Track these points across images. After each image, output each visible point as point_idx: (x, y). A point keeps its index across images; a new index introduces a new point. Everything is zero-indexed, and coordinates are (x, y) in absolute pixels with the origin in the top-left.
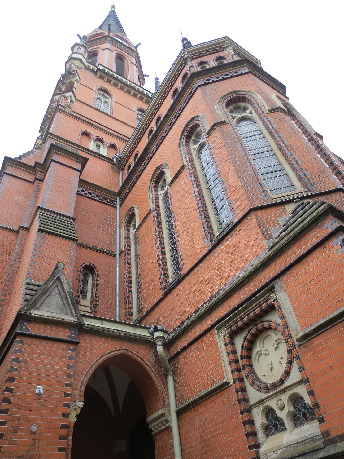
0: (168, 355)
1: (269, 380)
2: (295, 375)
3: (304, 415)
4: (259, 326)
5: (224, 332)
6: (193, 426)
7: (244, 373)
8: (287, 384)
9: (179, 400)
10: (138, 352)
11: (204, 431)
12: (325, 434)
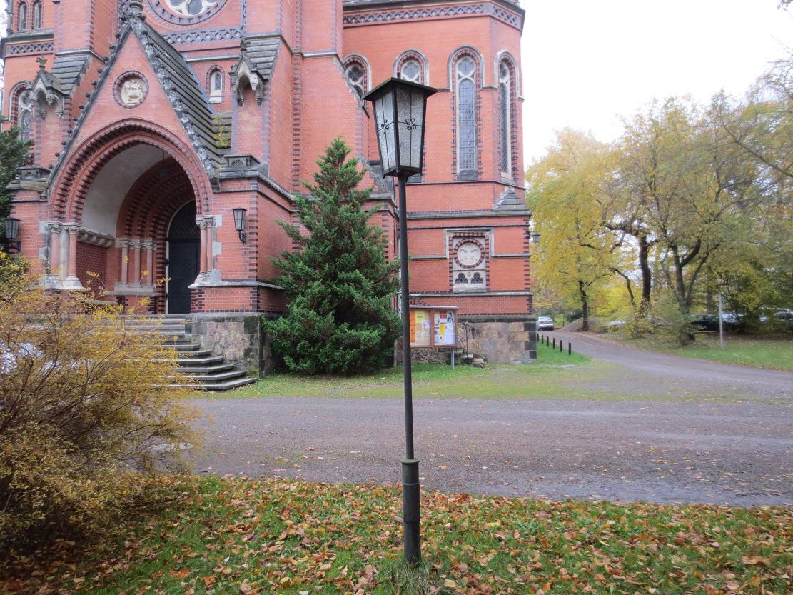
5: (451, 235)
8: (475, 269)
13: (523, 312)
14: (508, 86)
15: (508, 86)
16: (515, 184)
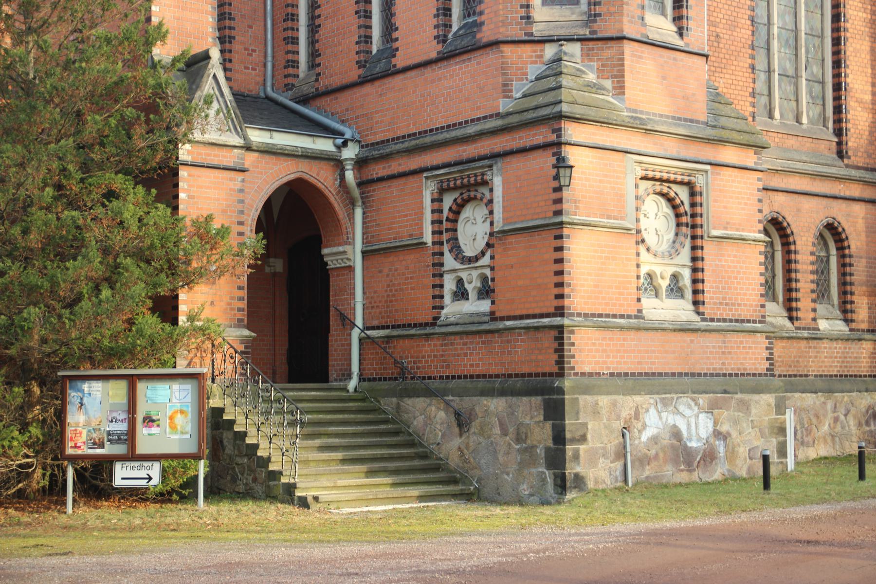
0: (359, 176)
1: (469, 252)
2: (486, 260)
3: (487, 292)
4: (472, 194)
6: (380, 272)
7: (445, 237)
9: (366, 239)
10: (318, 175)
11: (391, 281)
12: (492, 313)
13: (547, 370)
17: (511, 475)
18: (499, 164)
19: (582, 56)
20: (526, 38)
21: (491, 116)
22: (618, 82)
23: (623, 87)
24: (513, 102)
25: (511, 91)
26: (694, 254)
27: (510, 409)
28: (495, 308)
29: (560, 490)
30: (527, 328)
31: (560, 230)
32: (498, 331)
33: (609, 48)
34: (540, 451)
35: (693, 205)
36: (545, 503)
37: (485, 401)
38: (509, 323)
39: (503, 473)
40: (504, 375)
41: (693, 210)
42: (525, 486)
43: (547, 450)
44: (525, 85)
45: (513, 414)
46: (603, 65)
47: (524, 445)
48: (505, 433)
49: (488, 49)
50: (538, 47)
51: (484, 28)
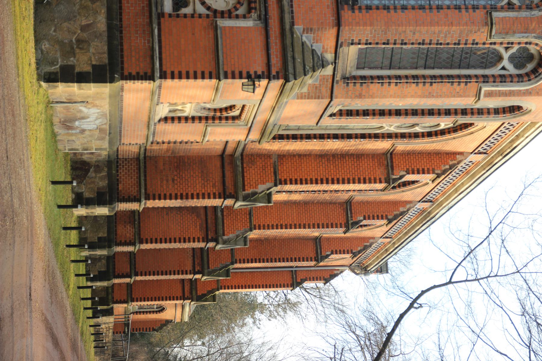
13: (126, 66)
14: (495, 71)
15: (495, 71)
16: (338, 77)
17: (54, 34)
18: (261, 25)
19: (324, 75)
20: (339, 43)
21: (293, 17)
22: (305, 96)
23: (302, 98)
24: (300, 33)
25: (307, 33)
26: (197, 118)
27: (98, 35)
28: (167, 16)
29: (47, 77)
30: (152, 49)
31: (215, 77)
32: (151, 23)
33: (327, 91)
34: (72, 61)
35: (227, 118)
36: (38, 63)
37: (104, 11)
38: (156, 31)
39: (55, 26)
40: (121, 27)
41: (223, 118)
42: (47, 46)
43: (73, 67)
44: (310, 41)
45: (96, 37)
46: (316, 87)
47: (75, 46)
48: (84, 28)
49: (335, 15)
50: (333, 50)
51: (350, 12)
